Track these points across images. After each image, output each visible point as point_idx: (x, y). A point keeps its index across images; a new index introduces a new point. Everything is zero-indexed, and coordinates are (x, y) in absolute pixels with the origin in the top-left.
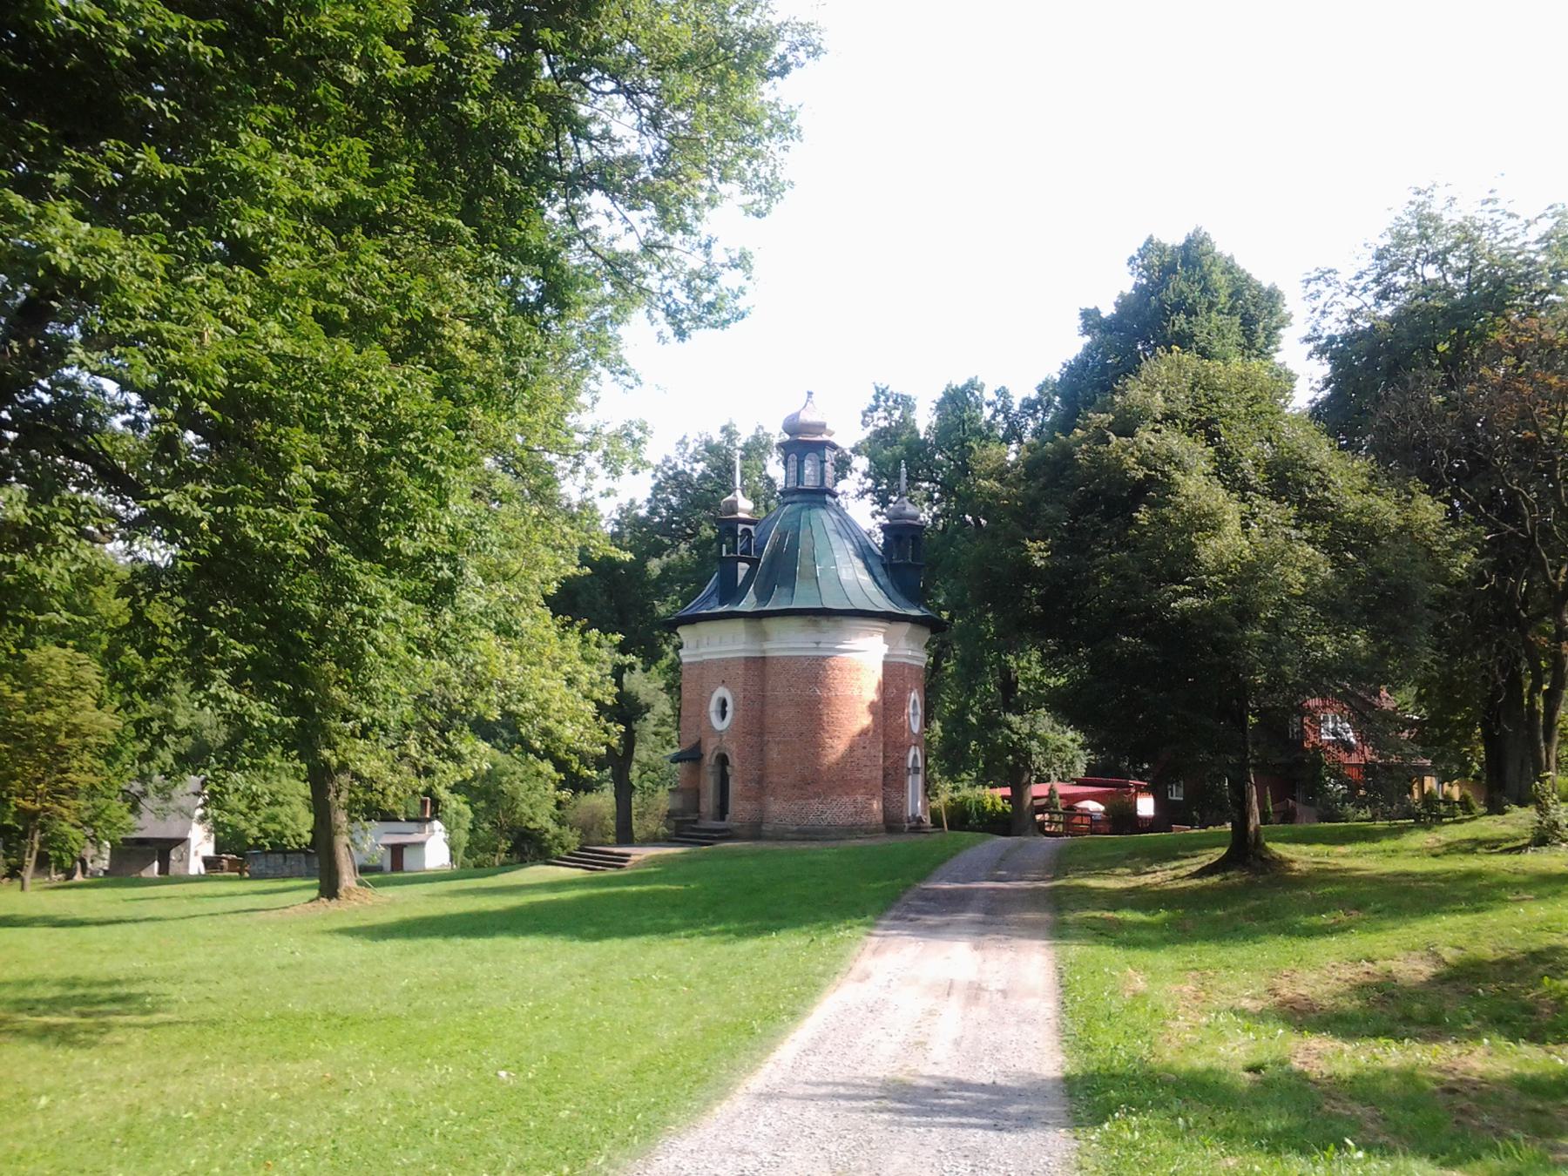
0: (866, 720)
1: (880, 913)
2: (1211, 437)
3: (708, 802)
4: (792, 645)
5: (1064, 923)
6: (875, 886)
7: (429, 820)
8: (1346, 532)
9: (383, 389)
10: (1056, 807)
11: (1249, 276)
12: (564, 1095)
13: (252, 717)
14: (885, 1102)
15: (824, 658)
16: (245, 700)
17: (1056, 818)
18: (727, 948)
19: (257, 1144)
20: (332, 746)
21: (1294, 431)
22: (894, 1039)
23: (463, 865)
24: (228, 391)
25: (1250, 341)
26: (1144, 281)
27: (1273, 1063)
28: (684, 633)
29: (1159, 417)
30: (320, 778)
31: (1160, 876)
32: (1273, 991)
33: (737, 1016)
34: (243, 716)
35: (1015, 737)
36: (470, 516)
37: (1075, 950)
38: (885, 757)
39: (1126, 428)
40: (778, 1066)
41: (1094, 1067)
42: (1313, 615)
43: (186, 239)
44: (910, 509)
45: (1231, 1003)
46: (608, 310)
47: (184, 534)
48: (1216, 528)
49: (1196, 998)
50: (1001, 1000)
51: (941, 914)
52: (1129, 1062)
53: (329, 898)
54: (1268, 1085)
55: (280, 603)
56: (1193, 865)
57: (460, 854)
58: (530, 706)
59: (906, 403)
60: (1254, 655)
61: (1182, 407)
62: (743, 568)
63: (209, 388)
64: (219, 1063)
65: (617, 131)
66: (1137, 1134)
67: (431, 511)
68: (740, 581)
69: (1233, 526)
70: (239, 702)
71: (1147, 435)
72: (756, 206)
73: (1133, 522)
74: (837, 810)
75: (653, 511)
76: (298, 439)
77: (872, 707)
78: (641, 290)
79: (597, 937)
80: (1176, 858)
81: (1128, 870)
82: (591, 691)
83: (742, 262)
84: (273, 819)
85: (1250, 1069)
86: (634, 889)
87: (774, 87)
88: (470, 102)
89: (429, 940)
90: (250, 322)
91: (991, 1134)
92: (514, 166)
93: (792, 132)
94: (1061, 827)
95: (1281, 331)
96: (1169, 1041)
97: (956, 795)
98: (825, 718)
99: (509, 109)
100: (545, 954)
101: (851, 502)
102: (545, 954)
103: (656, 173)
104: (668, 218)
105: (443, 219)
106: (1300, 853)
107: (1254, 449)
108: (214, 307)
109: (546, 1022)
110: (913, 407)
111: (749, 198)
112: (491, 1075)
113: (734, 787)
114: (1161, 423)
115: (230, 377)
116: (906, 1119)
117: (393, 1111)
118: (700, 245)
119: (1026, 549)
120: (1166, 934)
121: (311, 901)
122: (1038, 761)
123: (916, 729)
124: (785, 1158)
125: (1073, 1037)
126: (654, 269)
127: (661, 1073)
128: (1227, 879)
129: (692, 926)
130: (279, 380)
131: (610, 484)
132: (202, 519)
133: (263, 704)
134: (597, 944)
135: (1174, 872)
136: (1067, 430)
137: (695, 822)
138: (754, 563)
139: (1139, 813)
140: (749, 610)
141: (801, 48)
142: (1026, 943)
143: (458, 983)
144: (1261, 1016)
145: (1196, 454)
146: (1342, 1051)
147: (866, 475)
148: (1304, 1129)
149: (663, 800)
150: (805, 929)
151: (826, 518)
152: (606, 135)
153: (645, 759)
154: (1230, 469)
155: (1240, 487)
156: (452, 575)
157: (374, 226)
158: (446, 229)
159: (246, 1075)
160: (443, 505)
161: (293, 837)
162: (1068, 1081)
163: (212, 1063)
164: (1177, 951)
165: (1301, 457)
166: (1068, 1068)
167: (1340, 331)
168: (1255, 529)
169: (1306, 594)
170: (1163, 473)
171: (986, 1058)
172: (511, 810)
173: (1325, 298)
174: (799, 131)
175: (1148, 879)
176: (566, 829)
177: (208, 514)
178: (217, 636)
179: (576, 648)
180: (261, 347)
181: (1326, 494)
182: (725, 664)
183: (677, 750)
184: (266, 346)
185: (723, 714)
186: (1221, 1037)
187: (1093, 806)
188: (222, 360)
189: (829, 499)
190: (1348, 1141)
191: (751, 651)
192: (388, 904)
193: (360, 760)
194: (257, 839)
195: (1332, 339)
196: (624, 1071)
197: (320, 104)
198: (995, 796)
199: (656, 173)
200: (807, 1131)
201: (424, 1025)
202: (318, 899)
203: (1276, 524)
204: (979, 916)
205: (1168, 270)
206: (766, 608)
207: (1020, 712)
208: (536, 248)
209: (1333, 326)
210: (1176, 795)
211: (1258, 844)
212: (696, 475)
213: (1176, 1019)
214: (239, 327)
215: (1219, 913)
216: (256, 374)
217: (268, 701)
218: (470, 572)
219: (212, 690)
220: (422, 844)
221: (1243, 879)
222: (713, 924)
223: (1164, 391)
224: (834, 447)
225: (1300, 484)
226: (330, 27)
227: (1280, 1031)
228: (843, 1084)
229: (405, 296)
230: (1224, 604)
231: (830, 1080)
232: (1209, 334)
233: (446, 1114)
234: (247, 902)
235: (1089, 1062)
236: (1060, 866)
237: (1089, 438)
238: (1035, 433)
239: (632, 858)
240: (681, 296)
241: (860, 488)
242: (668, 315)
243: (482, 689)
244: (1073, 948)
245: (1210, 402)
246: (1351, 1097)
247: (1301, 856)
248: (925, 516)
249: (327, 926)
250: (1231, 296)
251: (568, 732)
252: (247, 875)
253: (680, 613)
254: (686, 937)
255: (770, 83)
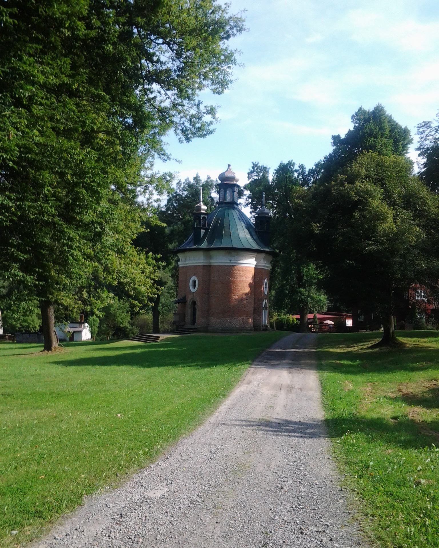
0: (247, 290)
1: (253, 360)
2: (383, 185)
3: (188, 318)
4: (221, 261)
5: (321, 364)
6: (251, 350)
7: (84, 323)
8: (432, 222)
9: (78, 157)
10: (316, 323)
11: (397, 124)
12: (142, 423)
13: (27, 281)
14: (260, 427)
15: (234, 266)
16: (25, 275)
17: (316, 326)
18: (198, 371)
19: (31, 439)
20: (52, 294)
21: (414, 183)
22: (262, 405)
23: (96, 340)
24: (19, 157)
25: (396, 149)
26: (357, 125)
27: (402, 416)
28: (180, 256)
29: (364, 177)
30: (44, 306)
31: (355, 348)
32: (400, 390)
33: (204, 396)
34: (24, 281)
35: (303, 297)
36: (107, 208)
37: (326, 374)
38: (255, 303)
39: (351, 180)
40: (220, 414)
41: (336, 417)
42: (419, 253)
43: (3, 98)
44: (266, 211)
45: (384, 394)
46: (157, 130)
47: (6, 212)
48: (384, 220)
49: (372, 392)
50: (300, 392)
51: (277, 360)
52: (349, 414)
53: (48, 351)
54: (401, 424)
55: (35, 240)
56: (369, 344)
57: (95, 335)
58: (128, 280)
59: (265, 170)
60: (396, 267)
61: (372, 174)
62: (203, 231)
63: (12, 155)
64: (13, 409)
65: (163, 59)
66: (355, 441)
67: (94, 206)
68: (201, 236)
69: (390, 220)
70: (23, 276)
71: (359, 184)
72: (218, 90)
73: (353, 217)
74: (237, 322)
75: (168, 209)
76: (47, 176)
77: (250, 285)
78: (172, 122)
79: (149, 367)
80: (362, 342)
81: (344, 346)
82: (150, 275)
83: (211, 111)
84: (25, 321)
85: (393, 418)
86: (162, 349)
87: (224, 43)
88: (109, 45)
89: (86, 367)
90: (27, 130)
91: (301, 439)
92: (126, 72)
93: (232, 61)
94: (318, 330)
95: (409, 146)
96: (363, 408)
97: (279, 317)
98: (233, 288)
99: (124, 48)
100: (130, 372)
101: (243, 207)
102: (130, 372)
103: (178, 76)
104: (182, 93)
105: (98, 92)
106: (408, 341)
107: (399, 190)
108: (13, 124)
109: (133, 397)
110: (268, 172)
111: (214, 87)
112: (115, 415)
113: (198, 313)
114: (364, 179)
115: (20, 151)
116: (269, 433)
117: (80, 428)
118: (195, 105)
119: (312, 226)
120: (359, 369)
121: (41, 351)
122: (310, 305)
123: (266, 293)
124: (226, 447)
125: (327, 407)
126: (177, 113)
127: (177, 415)
128: (381, 349)
129: (184, 363)
130: (39, 153)
131: (158, 197)
132: (12, 207)
133: (32, 277)
134: (149, 369)
135: (361, 347)
136: (329, 181)
137: (184, 326)
138: (207, 230)
139: (347, 325)
140: (205, 247)
141: (235, 28)
142: (308, 371)
143: (99, 382)
144: (395, 399)
145: (377, 192)
146: (427, 413)
147: (249, 197)
148: (415, 440)
149: (171, 317)
150: (226, 365)
151: (235, 213)
152: (158, 61)
153: (164, 302)
154: (389, 198)
155: (392, 204)
156: (101, 230)
157: (72, 94)
158: (99, 96)
159: (24, 414)
160: (98, 203)
161: (33, 328)
162: (327, 421)
163: (11, 410)
164: (364, 375)
165: (416, 193)
166: (326, 417)
167: (431, 146)
168: (399, 221)
169: (416, 245)
170: (365, 198)
171: (296, 412)
172: (114, 320)
173: (426, 133)
174: (235, 61)
175: (352, 349)
176: (134, 327)
177: (14, 205)
178: (14, 251)
179: (144, 259)
180: (31, 140)
181: (425, 208)
182: (196, 267)
183: (176, 299)
184: (33, 140)
185: (194, 286)
186: (381, 406)
187: (330, 322)
188: (17, 145)
189: (236, 206)
190: (433, 445)
191: (206, 263)
192: (70, 353)
193: (63, 299)
194: (19, 328)
195: (428, 149)
196: (163, 415)
197: (53, 44)
198: (294, 318)
199: (178, 76)
200: (233, 437)
201: (88, 397)
202: (44, 351)
203: (406, 218)
204: (290, 361)
205: (367, 121)
206: (211, 247)
207: (305, 288)
208: (133, 104)
209: (428, 144)
210: (361, 319)
211: (394, 338)
212: (184, 196)
213: (365, 400)
214: (23, 132)
215: (379, 362)
216: (29, 150)
217: (33, 275)
218: (107, 230)
219: (12, 272)
220: (81, 332)
221: (387, 350)
222: (192, 362)
223: (366, 167)
224: (238, 186)
225: (415, 204)
226: (58, 13)
227: (404, 405)
228: (245, 421)
229: (84, 122)
230: (386, 249)
231: (239, 419)
232: (381, 146)
233: (100, 429)
234: (17, 351)
235: (334, 415)
236: (319, 343)
237: (337, 185)
238: (314, 182)
239: (160, 338)
240: (187, 124)
241: (247, 202)
242: (183, 132)
243: (110, 274)
244: (326, 373)
245: (383, 172)
246: (431, 429)
247: (409, 342)
248: (271, 214)
249: (48, 361)
250: (390, 131)
251: (143, 289)
252: (15, 341)
253: (179, 248)
254: (182, 367)
255: (222, 42)
